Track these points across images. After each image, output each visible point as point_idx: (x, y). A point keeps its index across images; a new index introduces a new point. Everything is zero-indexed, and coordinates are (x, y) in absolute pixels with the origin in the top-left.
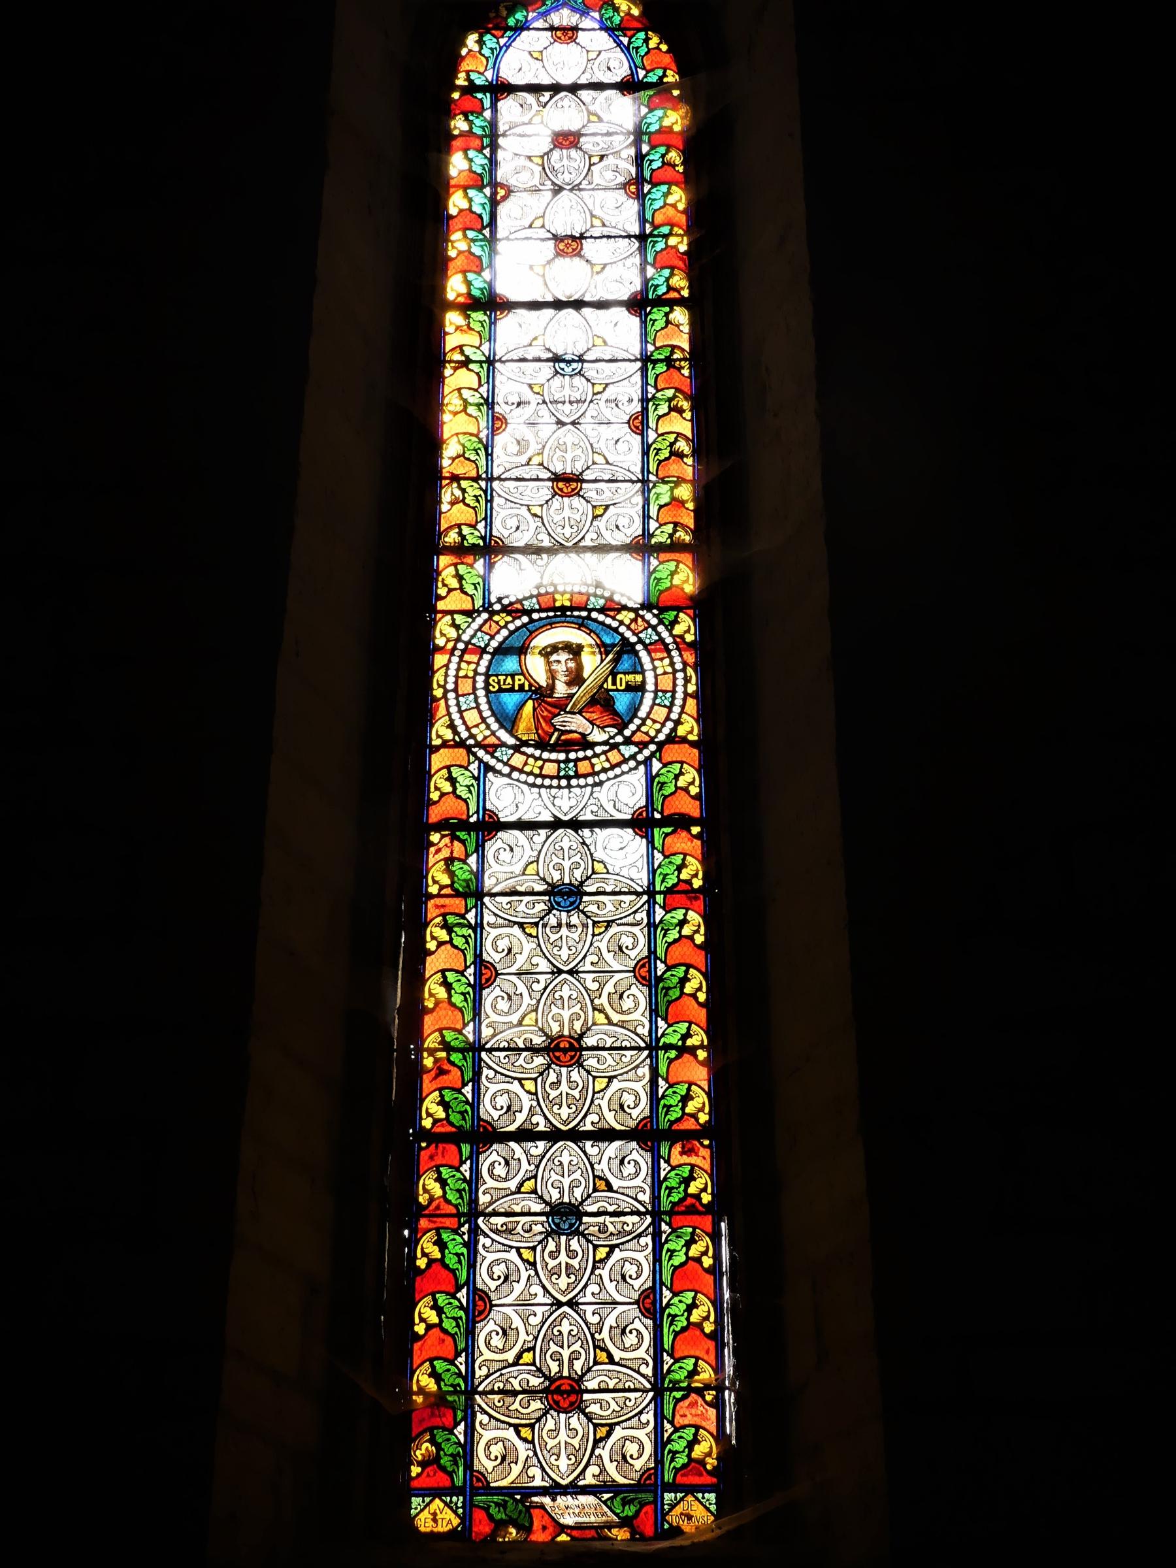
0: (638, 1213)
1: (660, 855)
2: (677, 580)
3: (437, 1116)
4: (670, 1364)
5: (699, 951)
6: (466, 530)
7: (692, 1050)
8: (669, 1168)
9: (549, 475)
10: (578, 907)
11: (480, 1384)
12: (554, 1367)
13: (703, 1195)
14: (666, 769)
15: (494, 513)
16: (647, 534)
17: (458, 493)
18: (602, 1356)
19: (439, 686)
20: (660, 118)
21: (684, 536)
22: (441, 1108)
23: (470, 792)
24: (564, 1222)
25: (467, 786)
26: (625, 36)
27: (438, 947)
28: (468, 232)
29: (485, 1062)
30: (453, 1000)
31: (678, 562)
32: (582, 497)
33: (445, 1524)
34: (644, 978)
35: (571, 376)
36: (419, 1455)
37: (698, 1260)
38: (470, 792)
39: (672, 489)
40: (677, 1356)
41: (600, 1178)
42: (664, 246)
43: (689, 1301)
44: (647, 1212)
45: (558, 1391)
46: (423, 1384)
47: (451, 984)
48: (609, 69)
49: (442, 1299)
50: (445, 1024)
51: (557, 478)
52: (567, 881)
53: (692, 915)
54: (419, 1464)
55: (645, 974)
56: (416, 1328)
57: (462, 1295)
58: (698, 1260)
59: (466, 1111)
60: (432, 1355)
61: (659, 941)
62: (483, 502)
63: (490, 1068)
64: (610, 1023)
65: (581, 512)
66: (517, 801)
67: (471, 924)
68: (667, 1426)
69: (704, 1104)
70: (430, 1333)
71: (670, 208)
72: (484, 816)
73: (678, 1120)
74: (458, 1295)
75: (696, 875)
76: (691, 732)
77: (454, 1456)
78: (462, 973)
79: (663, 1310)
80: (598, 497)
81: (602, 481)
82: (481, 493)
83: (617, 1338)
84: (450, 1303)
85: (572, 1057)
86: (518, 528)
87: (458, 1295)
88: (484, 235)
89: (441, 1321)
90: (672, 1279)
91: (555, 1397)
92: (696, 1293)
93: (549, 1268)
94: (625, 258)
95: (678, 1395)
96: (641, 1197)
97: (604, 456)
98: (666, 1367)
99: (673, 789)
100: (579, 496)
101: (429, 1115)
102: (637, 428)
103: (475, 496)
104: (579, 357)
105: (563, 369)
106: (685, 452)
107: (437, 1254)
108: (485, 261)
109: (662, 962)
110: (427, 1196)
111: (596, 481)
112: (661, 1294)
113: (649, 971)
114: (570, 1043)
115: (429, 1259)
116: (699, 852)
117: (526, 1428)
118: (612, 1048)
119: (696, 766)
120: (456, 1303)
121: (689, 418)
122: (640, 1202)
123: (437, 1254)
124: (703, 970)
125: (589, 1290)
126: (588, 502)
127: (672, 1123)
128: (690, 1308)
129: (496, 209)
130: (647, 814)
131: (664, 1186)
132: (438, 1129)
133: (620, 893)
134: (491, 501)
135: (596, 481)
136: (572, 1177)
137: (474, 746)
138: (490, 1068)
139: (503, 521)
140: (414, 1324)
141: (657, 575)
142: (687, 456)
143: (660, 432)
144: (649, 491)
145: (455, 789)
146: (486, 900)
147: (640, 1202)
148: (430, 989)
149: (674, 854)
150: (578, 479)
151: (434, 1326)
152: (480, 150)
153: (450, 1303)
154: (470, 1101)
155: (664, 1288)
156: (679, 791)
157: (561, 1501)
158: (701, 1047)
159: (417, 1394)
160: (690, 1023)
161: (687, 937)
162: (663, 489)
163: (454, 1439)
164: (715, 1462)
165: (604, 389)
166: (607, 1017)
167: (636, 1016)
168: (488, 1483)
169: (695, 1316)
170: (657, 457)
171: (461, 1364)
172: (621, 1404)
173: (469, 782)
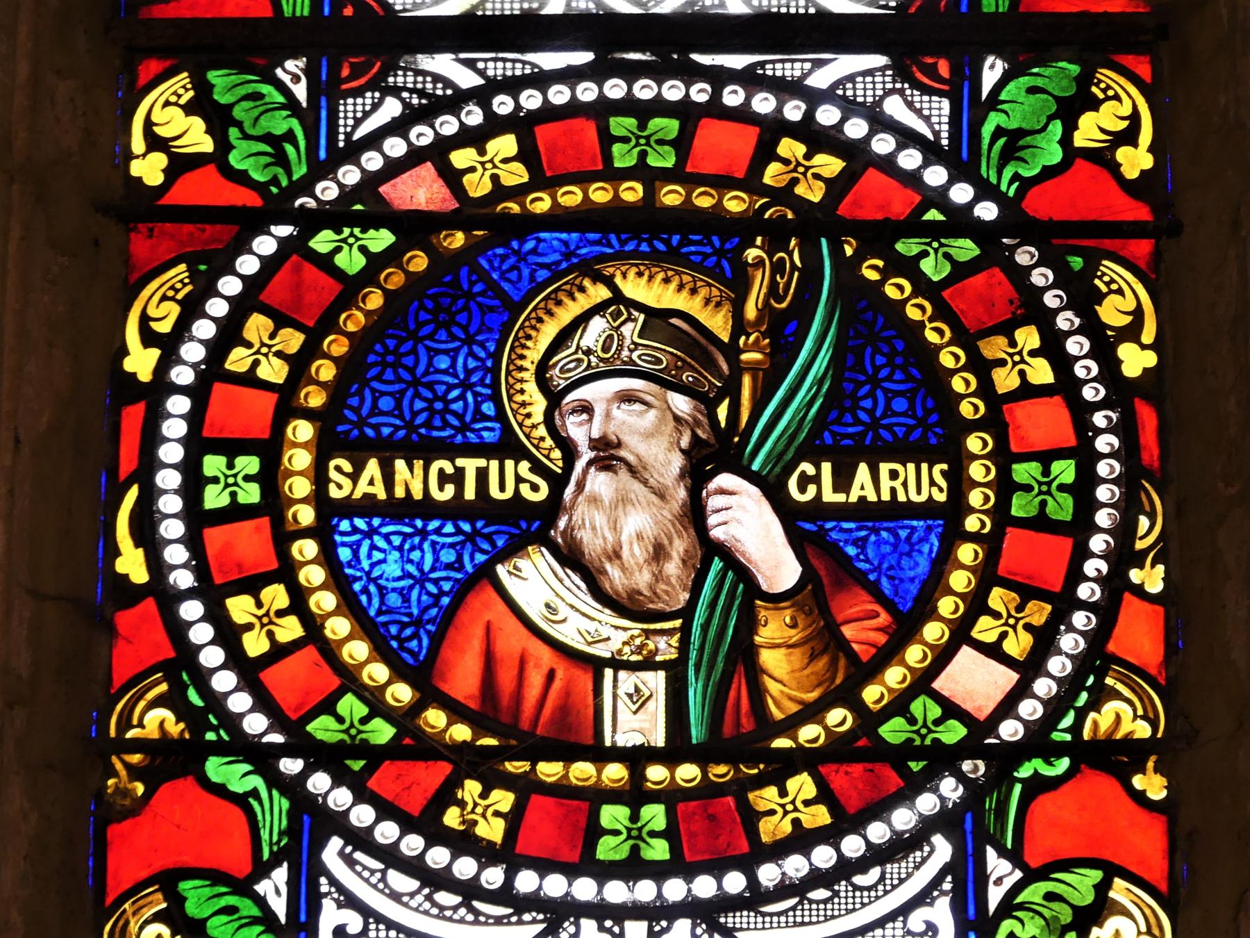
4: (1008, 883)
8: (1018, 875)
14: (1042, 887)
19: (150, 340)
29: (333, 881)
58: (1102, 158)
63: (349, 901)
68: (996, 864)
74: (263, 887)
78: (244, 887)
84: (230, 910)
87: (263, 887)
88: (261, 902)
98: (995, 896)
101: (155, 143)
110: (159, 160)
124: (1163, 887)
129: (332, 616)
131: (987, 130)
132: (185, 193)
138: (349, 901)
140: (129, 156)
145: (224, 147)
149: (1068, 865)
153: (257, 96)
156: (1080, 163)
164: (1147, 162)
171: (296, 79)
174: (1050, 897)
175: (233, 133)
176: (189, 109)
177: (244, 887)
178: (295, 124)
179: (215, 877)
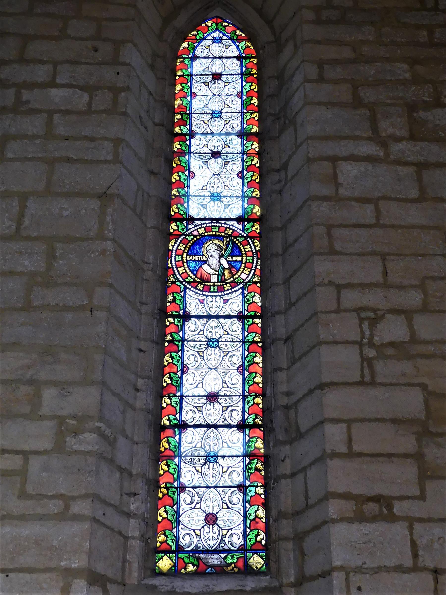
0: (238, 342)
1: (249, 529)
2: (254, 211)
3: (171, 322)
4: (249, 507)
5: (257, 184)
6: (174, 334)
7: (257, 343)
9: (209, 194)
10: (220, 117)
11: (183, 454)
12: (207, 447)
13: (263, 541)
14: (249, 294)
15: (190, 206)
16: (244, 420)
17: (181, 88)
18: (226, 333)
19: (172, 246)
20: (251, 129)
21: (259, 421)
22: (171, 359)
23: (185, 180)
24: (211, 518)
25: (176, 402)
26: (237, 42)
27: (164, 473)
28: (182, 84)
30: (180, 212)
31: (254, 157)
32: (222, 43)
33: (168, 565)
34: (240, 177)
35: (217, 118)
36: (169, 300)
37: (255, 180)
38: (185, 180)
39: (254, 399)
40: (251, 528)
41: (225, 331)
42: (252, 322)
43: (256, 533)
44: (241, 395)
45: (214, 196)
46: (165, 423)
47: (172, 377)
48: (233, 52)
49: (173, 354)
50: (167, 480)
51: (213, 113)
52: (217, 110)
53: (255, 143)
54: (160, 542)
55: (242, 369)
56: (160, 472)
57: (186, 173)
59: (178, 380)
60: (169, 414)
61: (245, 165)
62: (177, 471)
63: (186, 402)
64: (228, 387)
65: (221, 84)
66: (196, 308)
67: (177, 419)
69: (264, 537)
70: (167, 407)
71: (253, 150)
72: (180, 485)
73: (250, 150)
75: (258, 211)
76: (258, 195)
77: (180, 300)
79: (244, 176)
80: (227, 43)
81: (228, 113)
82: (176, 467)
83: (231, 65)
85: (218, 199)
86: (202, 52)
87: (181, 294)
89: (171, 403)
90: (248, 328)
91: (209, 398)
92: (259, 530)
93: (209, 306)
94: (238, 403)
95: (250, 343)
96: (238, 109)
97: (227, 331)
99: (252, 403)
100: (221, 118)
101: (172, 228)
102: (240, 97)
103: (184, 178)
104: (220, 111)
105: (211, 345)
106: (261, 469)
107: (171, 361)
108: (189, 66)
109: (248, 528)
110: (163, 448)
111: (226, 113)
112: (244, 312)
113: (242, 175)
114: (217, 195)
115: (163, 494)
116: (257, 124)
117: (199, 409)
118: (230, 342)
119: (257, 126)
120: (178, 336)
121: (264, 521)
122: (239, 339)
123: (171, 361)
125: (223, 171)
126: (224, 45)
127: (248, 151)
128: (252, 176)
130: (243, 423)
133: (233, 113)
134: (182, 404)
135: (226, 113)
136: (213, 503)
137: (183, 282)
139: (196, 88)
141: (246, 87)
142: (261, 471)
143: (250, 436)
144: (244, 115)
146: (193, 76)
147: (239, 339)
148: (160, 514)
150: (217, 341)
151: (166, 494)
152: (177, 352)
154: (181, 356)
155: (247, 528)
157: (210, 556)
158: (255, 74)
159: (173, 196)
160: (259, 530)
161: (251, 62)
162: (250, 398)
163: (175, 441)
165: (229, 84)
166: (228, 445)
167: (237, 386)
168: (184, 549)
169: (254, 178)
170: (248, 405)
172: (231, 522)
173: (181, 298)
174: (253, 533)
175: (173, 380)
176: (170, 357)
177: (179, 294)
178: (179, 379)
179: (177, 293)
